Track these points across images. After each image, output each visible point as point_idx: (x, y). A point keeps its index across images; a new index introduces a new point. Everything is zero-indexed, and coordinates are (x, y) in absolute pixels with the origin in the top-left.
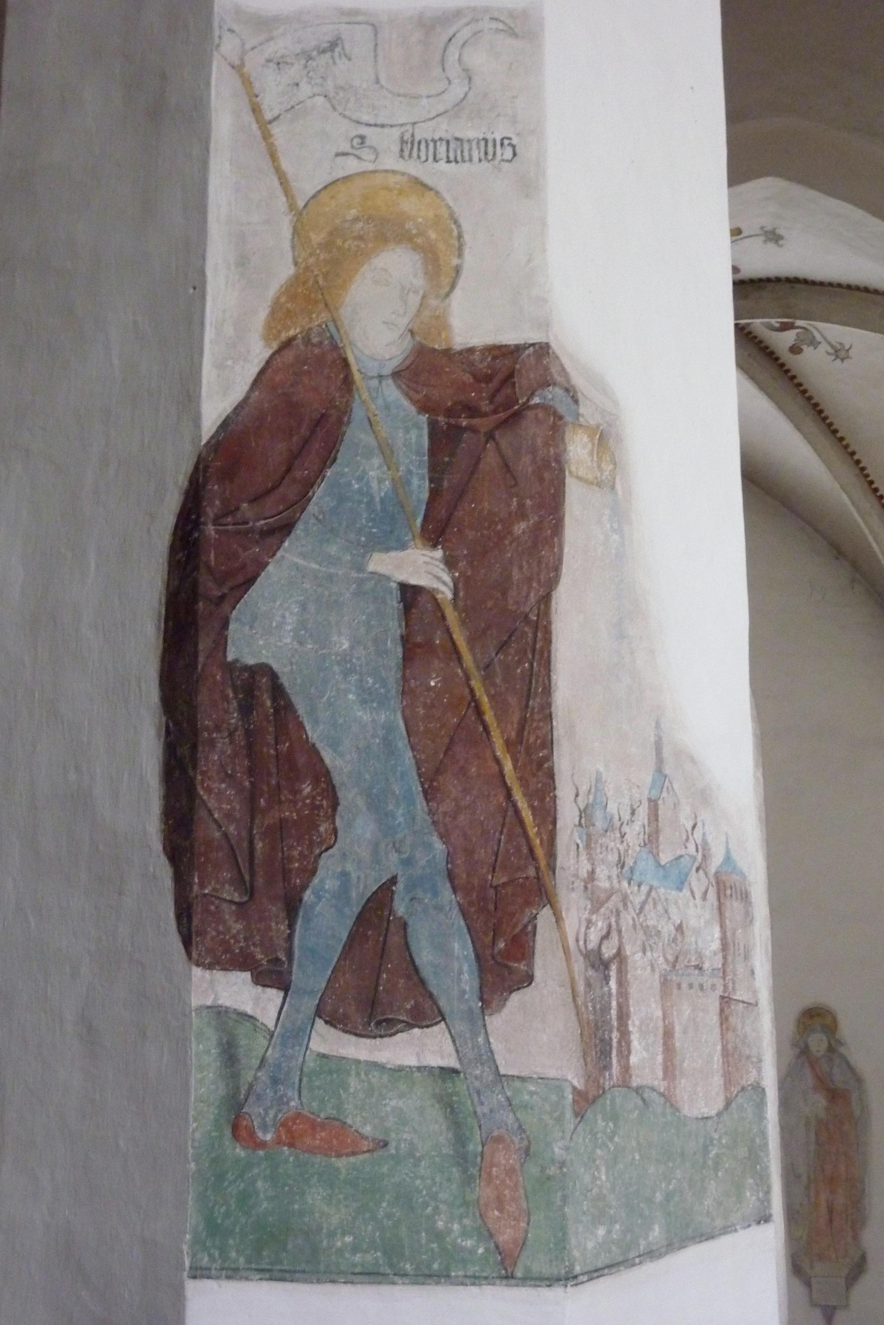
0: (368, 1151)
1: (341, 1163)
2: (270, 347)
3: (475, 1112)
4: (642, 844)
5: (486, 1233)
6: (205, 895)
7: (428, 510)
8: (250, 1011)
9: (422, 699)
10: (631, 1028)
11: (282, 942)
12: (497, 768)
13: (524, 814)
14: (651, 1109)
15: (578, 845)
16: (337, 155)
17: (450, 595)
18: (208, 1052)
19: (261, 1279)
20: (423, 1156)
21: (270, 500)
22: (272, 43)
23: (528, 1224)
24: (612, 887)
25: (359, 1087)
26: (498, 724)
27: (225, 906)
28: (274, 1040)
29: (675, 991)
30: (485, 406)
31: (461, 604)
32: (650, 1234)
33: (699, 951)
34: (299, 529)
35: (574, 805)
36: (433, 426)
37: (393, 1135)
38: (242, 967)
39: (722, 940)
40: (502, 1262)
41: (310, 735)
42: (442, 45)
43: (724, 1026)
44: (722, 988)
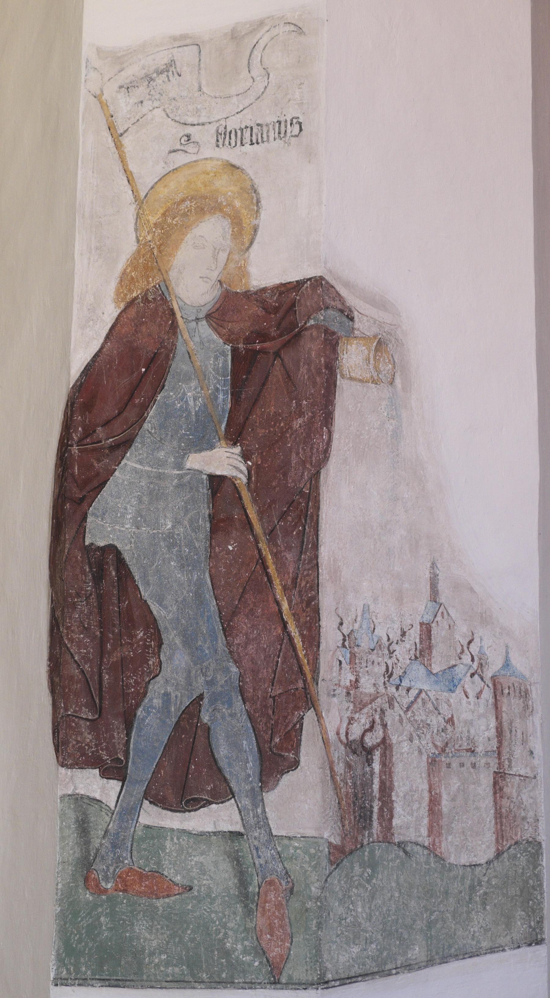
0: (178, 894)
1: (159, 903)
2: (119, 307)
3: (254, 863)
4: (413, 658)
5: (261, 952)
8: (98, 798)
15: (340, 662)
17: (245, 480)
18: (69, 827)
19: (102, 986)
20: (216, 896)
22: (123, 73)
23: (291, 944)
25: (173, 848)
27: (82, 722)
28: (114, 816)
29: (444, 769)
30: (273, 332)
31: (252, 486)
32: (409, 952)
34: (137, 444)
35: (338, 631)
36: (235, 351)
37: (196, 882)
39: (497, 728)
40: (271, 972)
41: (143, 593)
44: (496, 766)
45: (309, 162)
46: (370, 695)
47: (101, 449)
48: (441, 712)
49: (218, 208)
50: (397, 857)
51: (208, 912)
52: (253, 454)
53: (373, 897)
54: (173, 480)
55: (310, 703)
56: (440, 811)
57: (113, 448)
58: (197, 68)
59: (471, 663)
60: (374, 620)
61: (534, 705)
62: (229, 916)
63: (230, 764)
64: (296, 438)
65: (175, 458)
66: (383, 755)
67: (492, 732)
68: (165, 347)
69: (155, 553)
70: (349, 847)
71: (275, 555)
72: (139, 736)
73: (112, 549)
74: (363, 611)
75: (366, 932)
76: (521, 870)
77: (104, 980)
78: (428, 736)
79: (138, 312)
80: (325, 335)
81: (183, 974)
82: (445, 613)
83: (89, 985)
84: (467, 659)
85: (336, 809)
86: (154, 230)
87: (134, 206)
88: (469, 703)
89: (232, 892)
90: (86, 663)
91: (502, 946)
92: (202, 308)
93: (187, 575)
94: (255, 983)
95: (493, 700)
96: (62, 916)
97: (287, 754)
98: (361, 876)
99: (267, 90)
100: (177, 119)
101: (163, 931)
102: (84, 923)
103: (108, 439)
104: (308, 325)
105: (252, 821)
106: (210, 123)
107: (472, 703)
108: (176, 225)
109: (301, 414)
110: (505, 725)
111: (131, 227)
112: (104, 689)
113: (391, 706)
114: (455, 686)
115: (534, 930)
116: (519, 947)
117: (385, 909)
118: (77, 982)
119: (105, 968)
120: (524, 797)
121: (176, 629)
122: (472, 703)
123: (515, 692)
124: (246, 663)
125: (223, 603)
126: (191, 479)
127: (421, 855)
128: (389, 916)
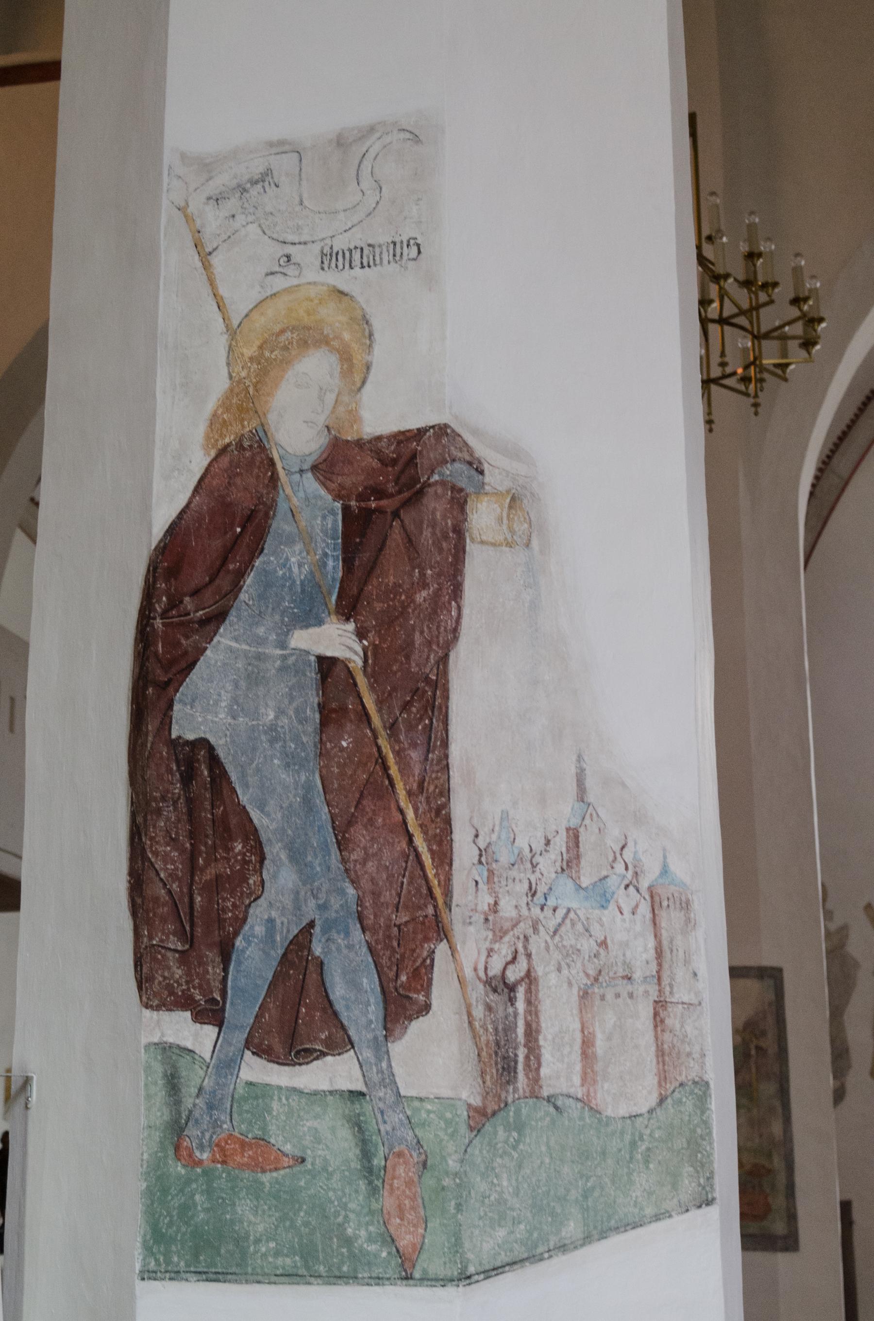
0: (289, 1167)
1: (266, 1178)
2: (209, 455)
3: (379, 1131)
4: (560, 870)
5: (389, 1239)
6: (153, 945)
7: (341, 589)
8: (190, 1047)
9: (336, 760)
10: (541, 1043)
11: (217, 984)
12: (401, 817)
13: (424, 858)
14: (565, 1115)
15: (477, 882)
16: (267, 275)
17: (360, 663)
18: (156, 1083)
19: (198, 1281)
20: (334, 1170)
21: (208, 594)
22: (211, 182)
23: (425, 1230)
24: (520, 916)
25: (281, 1110)
26: (402, 776)
27: (169, 954)
28: (210, 1070)
29: (597, 1002)
30: (391, 488)
31: (369, 670)
32: (563, 1229)
33: (628, 961)
34: (232, 617)
35: (474, 845)
36: (346, 509)
37: (309, 1152)
38: (184, 1007)
39: (656, 949)
40: (402, 1265)
41: (240, 797)
42: (357, 162)
43: (659, 1029)
44: (657, 993)
45: (430, 290)
46: (512, 920)
47: (189, 623)
48: (593, 933)
49: (324, 341)
50: (547, 1114)
51: (324, 1190)
52: (368, 631)
53: (520, 1166)
54: (274, 662)
55: (442, 934)
56: (594, 1055)
57: (204, 622)
58: (297, 178)
59: (625, 872)
60: (515, 829)
61: (697, 918)
62: (350, 1195)
63: (348, 1008)
64: (419, 614)
65: (278, 635)
66: (529, 991)
67: (652, 953)
68: (264, 504)
69: (254, 749)
70: (491, 1107)
71: (398, 754)
72: (238, 971)
73: (203, 743)
74: (502, 818)
75: (512, 1209)
76: (687, 1118)
77: (200, 1273)
78: (579, 964)
79: (231, 462)
80: (452, 492)
81: (296, 1267)
82: (594, 815)
83: (182, 1279)
84: (620, 867)
85: (476, 1062)
86: (249, 364)
87: (226, 336)
88: (624, 920)
89: (353, 1165)
90: (173, 882)
91: (668, 1212)
92: (307, 458)
93: (293, 776)
94: (382, 1278)
95: (651, 916)
96: (149, 1192)
97: (415, 996)
98: (506, 1142)
99: (380, 205)
100: (275, 236)
101: (271, 1213)
102: (176, 1203)
103: (197, 611)
104: (432, 480)
105: (376, 1078)
106: (313, 242)
107: (627, 920)
108: (275, 360)
109: (425, 586)
110: (665, 943)
111: (223, 361)
112: (196, 914)
113: (535, 930)
114: (608, 901)
115: (704, 1188)
116: (687, 1210)
117: (534, 1180)
118: (168, 1275)
119: (201, 1258)
120: (689, 1029)
121: (281, 840)
122: (627, 920)
123: (675, 903)
124: (365, 883)
125: (337, 811)
126: (297, 661)
127: (574, 1109)
128: (538, 1187)
